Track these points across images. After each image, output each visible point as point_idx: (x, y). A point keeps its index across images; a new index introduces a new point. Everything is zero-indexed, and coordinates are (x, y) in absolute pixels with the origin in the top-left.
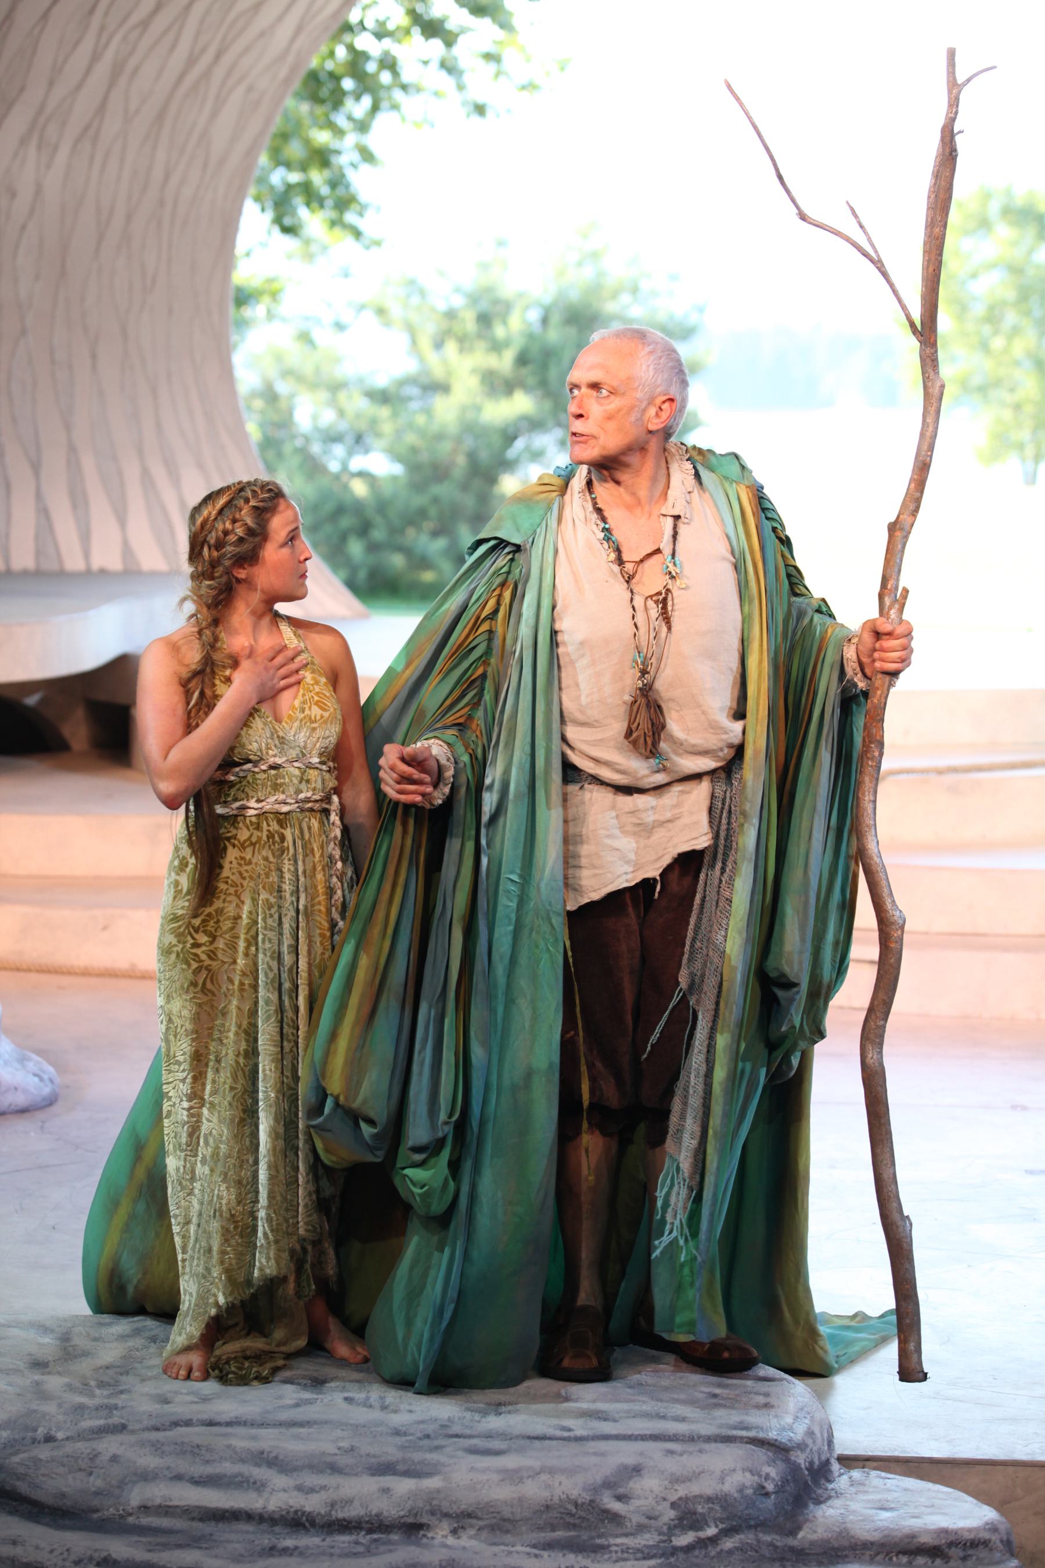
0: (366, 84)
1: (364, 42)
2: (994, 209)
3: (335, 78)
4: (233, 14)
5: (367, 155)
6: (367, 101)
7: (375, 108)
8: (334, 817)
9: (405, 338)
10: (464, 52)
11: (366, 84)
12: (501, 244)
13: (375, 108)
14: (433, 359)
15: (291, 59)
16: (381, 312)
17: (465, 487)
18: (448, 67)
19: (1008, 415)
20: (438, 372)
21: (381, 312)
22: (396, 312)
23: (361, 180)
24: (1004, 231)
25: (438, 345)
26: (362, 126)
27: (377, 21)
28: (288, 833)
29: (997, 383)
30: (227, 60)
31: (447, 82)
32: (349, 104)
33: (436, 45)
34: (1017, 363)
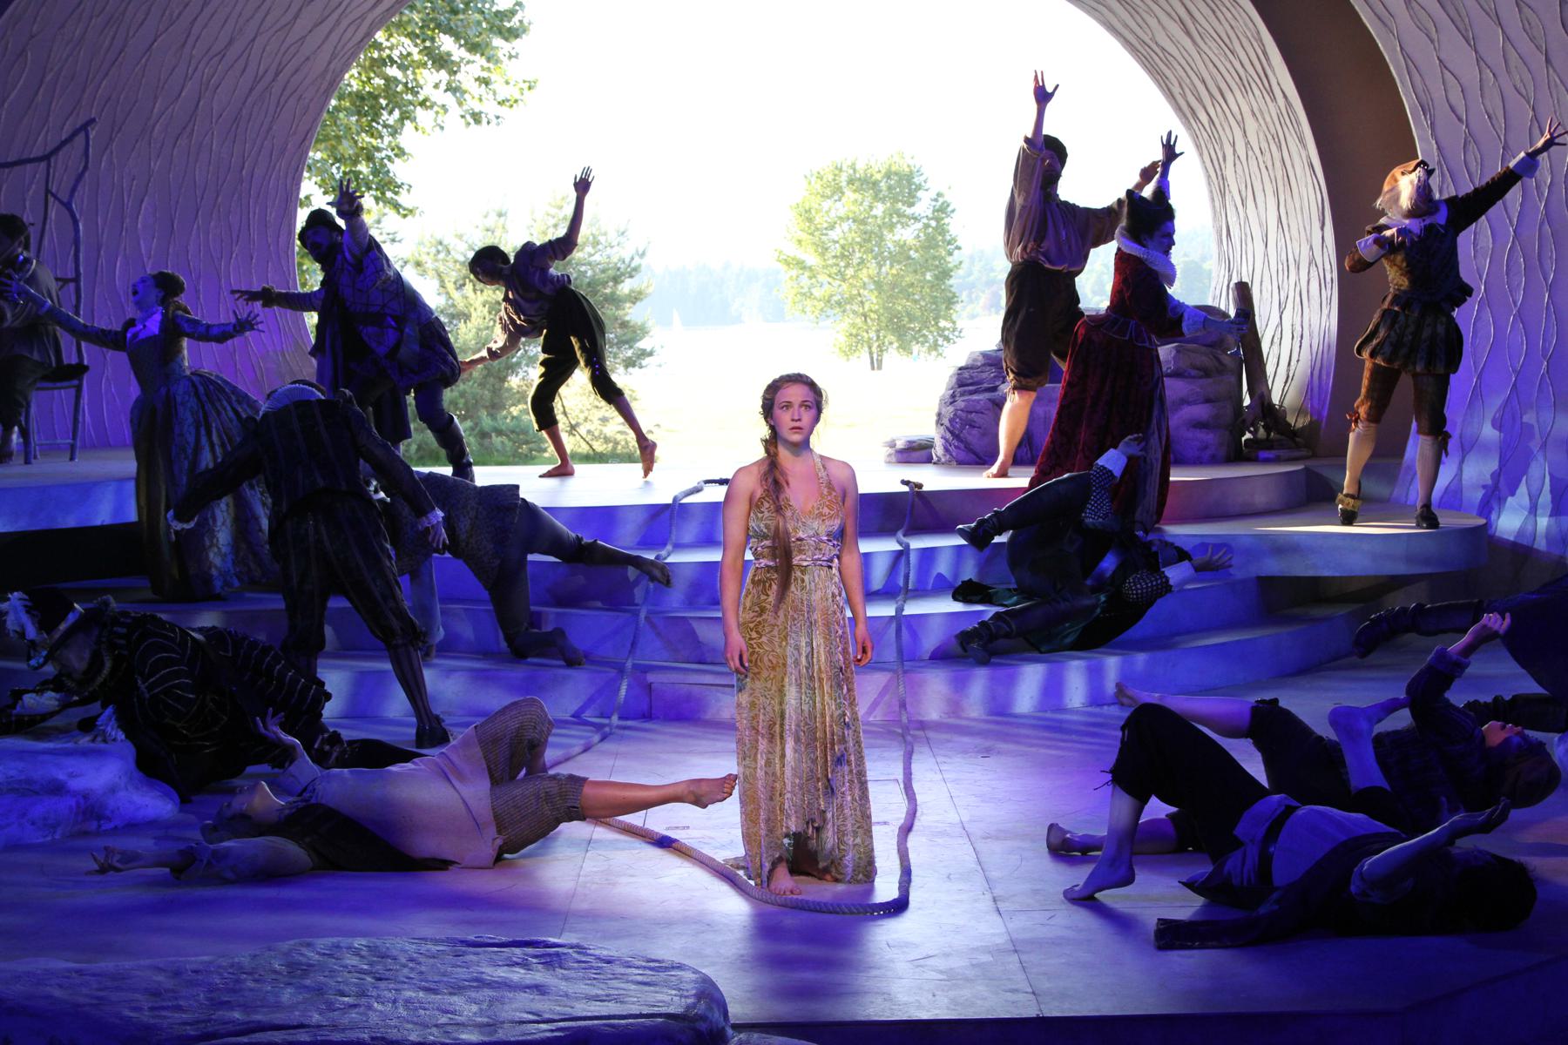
0: (395, 102)
1: (393, 71)
2: (844, 178)
3: (374, 97)
4: (286, 45)
5: (400, 153)
6: (397, 114)
7: (402, 119)
8: (834, 571)
9: (436, 283)
10: (466, 78)
11: (395, 102)
12: (500, 215)
13: (402, 119)
14: (456, 295)
15: (328, 77)
16: (418, 264)
17: (482, 385)
18: (452, 89)
19: (859, 321)
20: (461, 305)
21: (418, 264)
22: (429, 265)
23: (398, 169)
24: (850, 195)
25: (460, 287)
26: (394, 132)
27: (892, 445)
28: (806, 578)
29: (851, 300)
30: (282, 78)
31: (449, 99)
32: (385, 115)
33: (443, 75)
34: (864, 286)
